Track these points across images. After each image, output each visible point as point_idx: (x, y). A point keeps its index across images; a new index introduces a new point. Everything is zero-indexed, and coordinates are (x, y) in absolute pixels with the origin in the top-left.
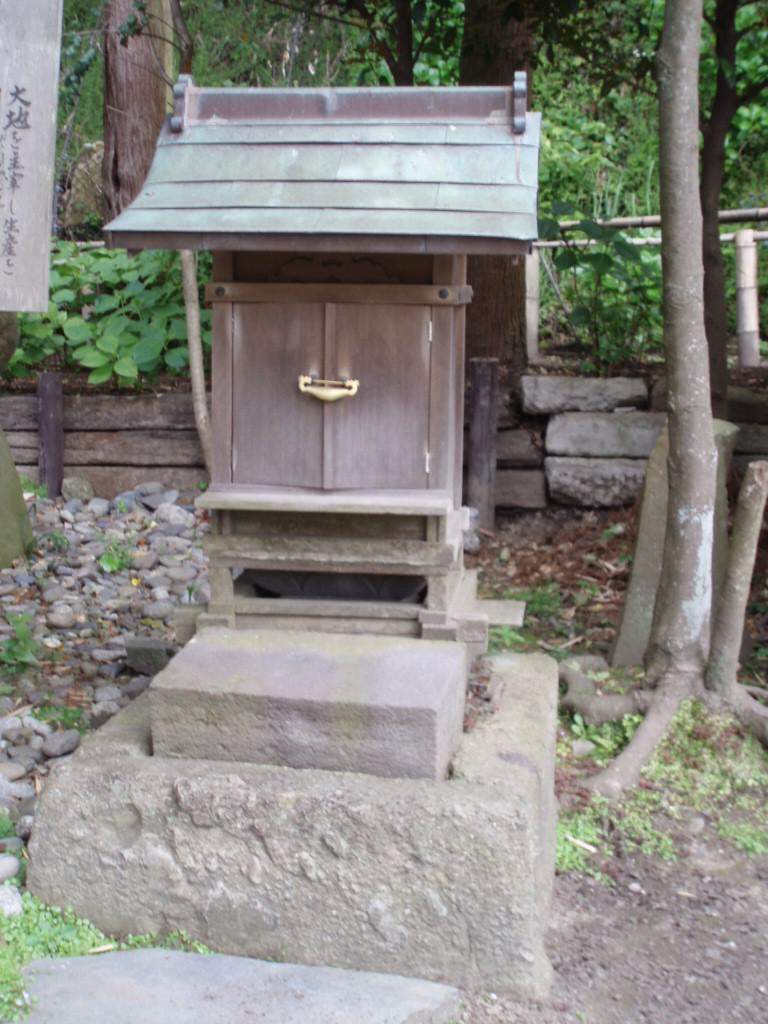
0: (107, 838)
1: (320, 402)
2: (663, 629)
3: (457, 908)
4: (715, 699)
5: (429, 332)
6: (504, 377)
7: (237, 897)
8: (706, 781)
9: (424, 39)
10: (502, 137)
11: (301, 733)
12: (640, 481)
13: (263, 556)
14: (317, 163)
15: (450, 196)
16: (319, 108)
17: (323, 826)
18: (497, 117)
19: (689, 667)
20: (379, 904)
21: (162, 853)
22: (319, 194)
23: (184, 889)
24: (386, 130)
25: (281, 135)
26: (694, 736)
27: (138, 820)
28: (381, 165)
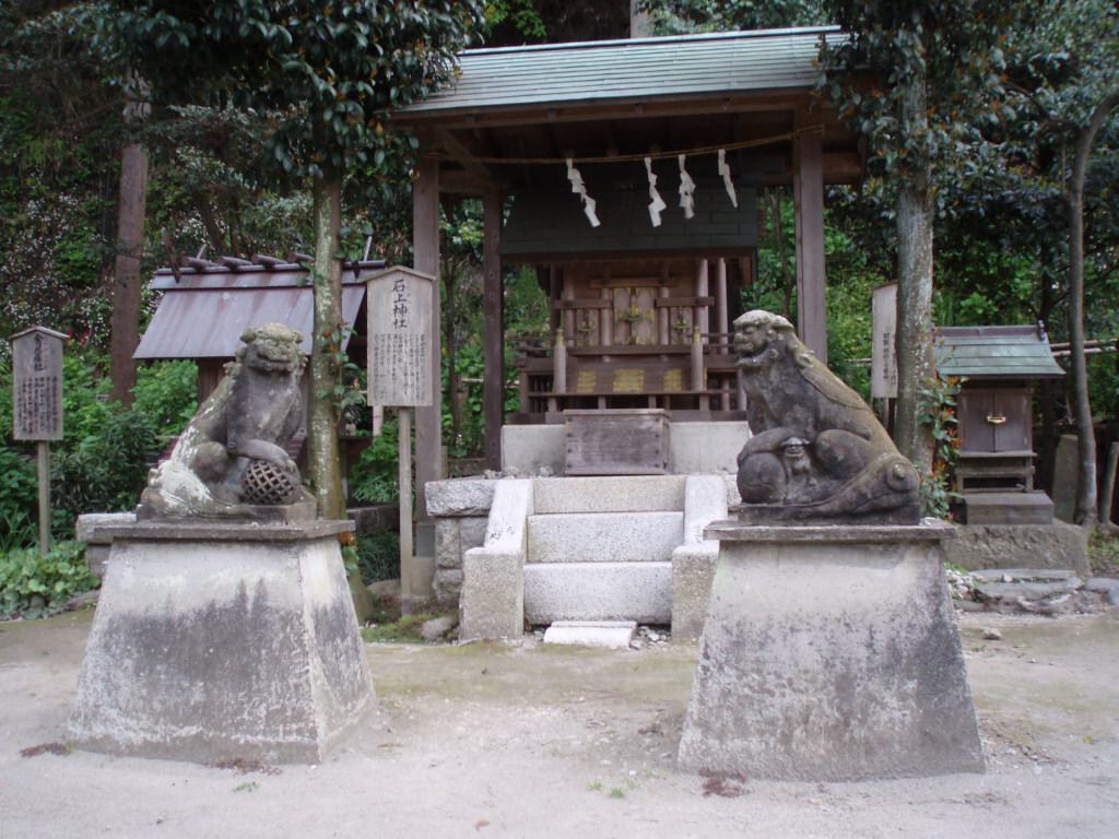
0: (967, 544)
1: (993, 424)
2: (1082, 504)
3: (1069, 554)
4: (1103, 525)
5: (1025, 402)
6: (356, 532)
7: (1007, 556)
8: (1105, 551)
9: (403, 57)
10: (1037, 342)
11: (1013, 515)
12: (735, 631)
13: (972, 473)
14: (983, 351)
15: (1030, 361)
16: (977, 333)
17: (1031, 534)
18: (1034, 335)
19: (1093, 515)
20: (1048, 555)
21: (985, 546)
22: (992, 362)
23: (992, 556)
24: (1000, 340)
25: (967, 342)
26: (1097, 538)
27: (976, 536)
28: (1004, 352)
